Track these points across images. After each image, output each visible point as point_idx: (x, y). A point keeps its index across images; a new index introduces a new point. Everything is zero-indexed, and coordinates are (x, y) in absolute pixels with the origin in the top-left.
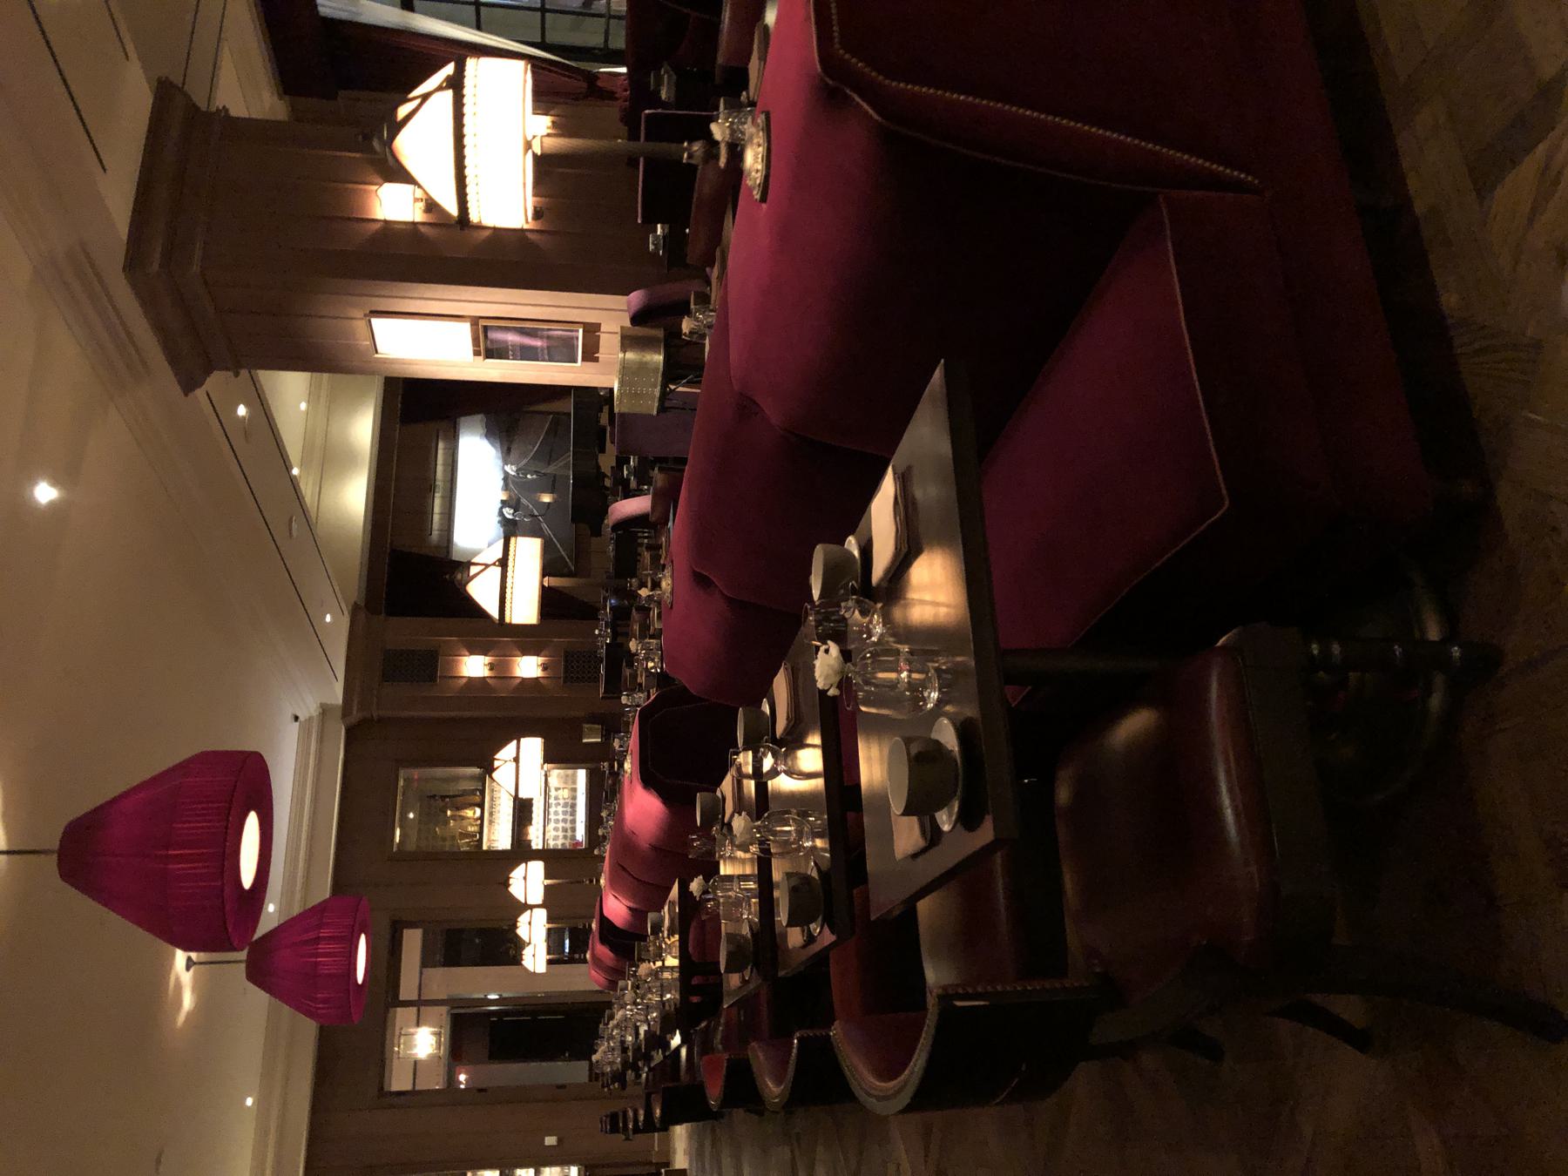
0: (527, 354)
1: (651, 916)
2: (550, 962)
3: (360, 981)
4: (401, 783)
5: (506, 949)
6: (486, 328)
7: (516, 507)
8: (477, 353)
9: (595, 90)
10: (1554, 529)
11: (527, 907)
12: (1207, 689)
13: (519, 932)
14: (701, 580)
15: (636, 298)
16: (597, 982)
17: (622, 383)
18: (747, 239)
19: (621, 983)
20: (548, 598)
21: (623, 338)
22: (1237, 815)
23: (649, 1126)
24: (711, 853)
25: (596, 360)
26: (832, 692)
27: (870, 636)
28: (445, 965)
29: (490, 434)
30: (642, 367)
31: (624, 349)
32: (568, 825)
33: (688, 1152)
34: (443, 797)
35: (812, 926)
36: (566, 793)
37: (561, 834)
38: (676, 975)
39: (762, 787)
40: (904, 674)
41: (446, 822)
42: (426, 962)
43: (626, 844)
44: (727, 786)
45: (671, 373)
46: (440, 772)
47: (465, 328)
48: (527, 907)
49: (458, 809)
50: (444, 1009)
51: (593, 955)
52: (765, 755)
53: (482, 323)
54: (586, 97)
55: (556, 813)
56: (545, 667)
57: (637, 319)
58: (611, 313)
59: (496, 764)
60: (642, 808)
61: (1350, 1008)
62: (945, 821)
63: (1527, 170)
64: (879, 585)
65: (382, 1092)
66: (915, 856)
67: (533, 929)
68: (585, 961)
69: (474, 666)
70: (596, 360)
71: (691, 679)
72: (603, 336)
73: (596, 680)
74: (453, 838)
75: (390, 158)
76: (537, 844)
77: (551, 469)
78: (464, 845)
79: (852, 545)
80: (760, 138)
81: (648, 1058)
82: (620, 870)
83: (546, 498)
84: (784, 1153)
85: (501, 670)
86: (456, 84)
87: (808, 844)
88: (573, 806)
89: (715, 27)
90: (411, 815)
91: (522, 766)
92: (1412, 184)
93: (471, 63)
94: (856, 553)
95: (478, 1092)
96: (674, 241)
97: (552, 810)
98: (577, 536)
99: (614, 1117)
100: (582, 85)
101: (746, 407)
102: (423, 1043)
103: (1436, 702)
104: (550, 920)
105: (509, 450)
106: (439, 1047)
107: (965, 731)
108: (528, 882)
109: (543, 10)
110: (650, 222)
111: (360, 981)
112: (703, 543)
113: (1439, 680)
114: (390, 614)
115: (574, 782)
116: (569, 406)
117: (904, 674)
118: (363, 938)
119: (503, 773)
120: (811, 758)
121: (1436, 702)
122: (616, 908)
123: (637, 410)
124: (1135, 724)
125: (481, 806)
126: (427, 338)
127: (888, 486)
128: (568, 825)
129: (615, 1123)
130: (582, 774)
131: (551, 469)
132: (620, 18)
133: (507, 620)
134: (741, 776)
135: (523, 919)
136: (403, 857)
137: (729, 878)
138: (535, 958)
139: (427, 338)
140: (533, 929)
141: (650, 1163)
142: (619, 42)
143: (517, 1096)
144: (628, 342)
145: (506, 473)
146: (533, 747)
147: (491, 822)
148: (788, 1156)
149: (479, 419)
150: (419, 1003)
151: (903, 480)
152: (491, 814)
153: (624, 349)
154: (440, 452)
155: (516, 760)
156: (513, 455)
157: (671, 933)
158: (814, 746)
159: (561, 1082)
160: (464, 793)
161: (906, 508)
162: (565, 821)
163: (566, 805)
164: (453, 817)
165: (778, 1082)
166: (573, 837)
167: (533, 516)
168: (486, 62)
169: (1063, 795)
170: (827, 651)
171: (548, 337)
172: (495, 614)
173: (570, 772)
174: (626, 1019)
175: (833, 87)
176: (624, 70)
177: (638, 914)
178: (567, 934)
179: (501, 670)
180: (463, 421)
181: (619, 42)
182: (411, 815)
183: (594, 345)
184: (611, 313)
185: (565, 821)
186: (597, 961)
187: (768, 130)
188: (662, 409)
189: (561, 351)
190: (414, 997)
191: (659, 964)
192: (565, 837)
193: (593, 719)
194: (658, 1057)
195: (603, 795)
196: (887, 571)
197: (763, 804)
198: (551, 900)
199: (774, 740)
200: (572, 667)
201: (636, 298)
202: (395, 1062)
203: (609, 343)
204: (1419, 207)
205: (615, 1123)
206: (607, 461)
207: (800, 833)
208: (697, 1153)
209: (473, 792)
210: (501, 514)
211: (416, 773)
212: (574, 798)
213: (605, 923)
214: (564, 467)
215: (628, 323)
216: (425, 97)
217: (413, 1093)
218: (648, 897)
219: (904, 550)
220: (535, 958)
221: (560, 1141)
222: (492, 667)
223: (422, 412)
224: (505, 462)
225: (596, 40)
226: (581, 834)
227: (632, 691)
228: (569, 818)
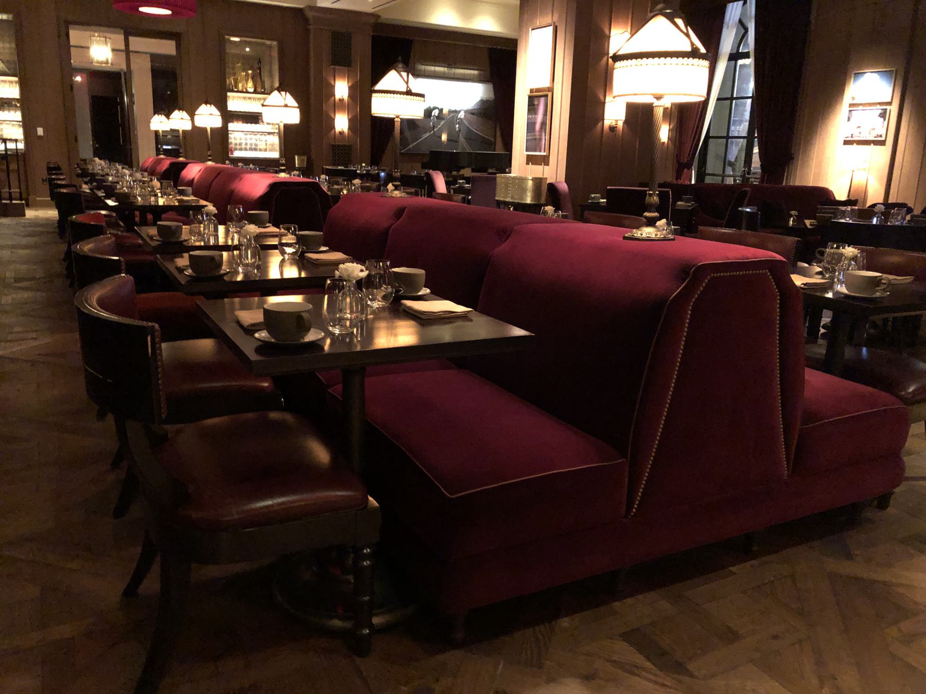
0: (531, 126)
1: (189, 190)
2: (156, 132)
3: (141, 9)
4: (268, 42)
5: (164, 106)
6: (546, 96)
7: (440, 117)
8: (532, 91)
9: (682, 167)
10: (437, 680)
11: (192, 115)
12: (344, 489)
13: (176, 112)
14: (400, 212)
15: (563, 187)
16: (143, 164)
17: (514, 178)
18: (599, 232)
19: (146, 174)
20: (386, 124)
21: (540, 179)
22: (267, 507)
23: (53, 186)
24: (231, 220)
25: (527, 164)
26: (337, 272)
27: (371, 300)
28: (152, 66)
29: (483, 102)
30: (523, 190)
31: (534, 179)
32: (243, 146)
33: (37, 218)
34: (260, 69)
35: (190, 271)
36: (263, 146)
37: (238, 142)
38: (153, 203)
39: (274, 247)
40: (349, 316)
41: (244, 71)
42: (154, 57)
43: (234, 176)
44: (272, 229)
45: (521, 207)
46: (276, 67)
47: (546, 84)
48: (192, 115)
49: (253, 78)
50: (124, 67)
51: (162, 159)
52: (294, 247)
53: (550, 94)
54: (678, 161)
55: (251, 139)
56: (341, 133)
57: (552, 188)
58: (555, 172)
59: (283, 93)
60: (256, 185)
61: (151, 585)
62: (262, 335)
63: (640, 659)
64: (402, 304)
65: (68, 24)
66: (238, 322)
67: (179, 121)
68: (158, 154)
69: (342, 89)
70: (527, 164)
71: (336, 210)
72: (541, 167)
73: (334, 165)
74: (234, 74)
75: (652, 14)
76: (232, 126)
77: (462, 139)
78: (230, 81)
79: (425, 291)
80: (660, 235)
81: (99, 188)
82: (218, 173)
83: (444, 137)
84: (40, 274)
85: (340, 105)
86: (694, 54)
87: (240, 269)
88: (255, 150)
89: (721, 226)
90: (248, 49)
91: (282, 110)
92: (629, 601)
93: (706, 63)
94: (420, 293)
95: (72, 86)
96: (596, 207)
97: (252, 136)
98: (423, 155)
99: (58, 168)
100: (685, 160)
101: (504, 233)
102: (101, 51)
103: (337, 623)
104: (184, 131)
105: (473, 114)
106: (98, 62)
107: (316, 346)
108: (208, 117)
109: (728, 137)
110: (608, 194)
111: (141, 9)
112: (422, 212)
113: (347, 625)
114: (374, 39)
115: (271, 150)
116: (500, 150)
117: (349, 316)
118: (169, 12)
119: (276, 97)
120: (292, 272)
121: (337, 623)
122: (194, 171)
123: (498, 187)
124: (321, 454)
125: (255, 92)
126: (541, 63)
127: (460, 309)
128: (243, 146)
129: (53, 169)
130: (276, 155)
131: (462, 139)
132: (723, 181)
133: (374, 95)
134: (280, 236)
135: (184, 114)
136: (222, 43)
137: (216, 230)
138: (159, 123)
139: (541, 63)
140: (179, 121)
141: (29, 195)
142: (708, 180)
143: (69, 113)
144: (538, 182)
145: (459, 112)
146: (294, 117)
147: (245, 98)
148: (38, 276)
149: (491, 96)
150: (127, 51)
151: (464, 317)
152: (250, 98)
153: (534, 179)
154: (472, 72)
155: (286, 106)
156: (469, 116)
157: (179, 201)
158: (300, 274)
159: (79, 138)
160: (263, 83)
161: (448, 318)
162: (246, 144)
163: (256, 145)
164: (247, 75)
165: (90, 250)
166: (236, 149)
167: (434, 127)
168: (707, 71)
169: (274, 415)
170: (362, 271)
171: (541, 135)
172: (377, 87)
173: (277, 148)
174: (123, 176)
175: (690, 273)
176: (693, 182)
177: (190, 183)
178: (174, 147)
179: (340, 105)
180: (491, 86)
181: (708, 180)
182: (248, 49)
183: (537, 161)
184: (555, 172)
185: (246, 144)
186: (159, 162)
187: (664, 239)
188: (499, 203)
189: (533, 143)
190: (131, 48)
191: (159, 195)
192: (236, 144)
193: (309, 161)
194: (101, 194)
195: (264, 165)
196: (410, 308)
197: (262, 249)
198: (198, 132)
199: (303, 253)
200: (342, 151)
201: (563, 187)
202: (87, 33)
203: (537, 171)
204: (617, 605)
205: (53, 169)
206: (467, 172)
207: (247, 265)
208: (35, 223)
209: (263, 87)
210: (435, 108)
211: (275, 54)
212: (260, 150)
213: (184, 165)
214: (463, 146)
215: (548, 182)
216: (687, 35)
217: (68, 47)
218: (203, 189)
219: (423, 317)
220: (159, 123)
221: (40, 136)
222: (341, 100)
223: (495, 60)
224: (466, 112)
225: (709, 169)
226: (237, 154)
227: (329, 182)
228: (248, 147)
